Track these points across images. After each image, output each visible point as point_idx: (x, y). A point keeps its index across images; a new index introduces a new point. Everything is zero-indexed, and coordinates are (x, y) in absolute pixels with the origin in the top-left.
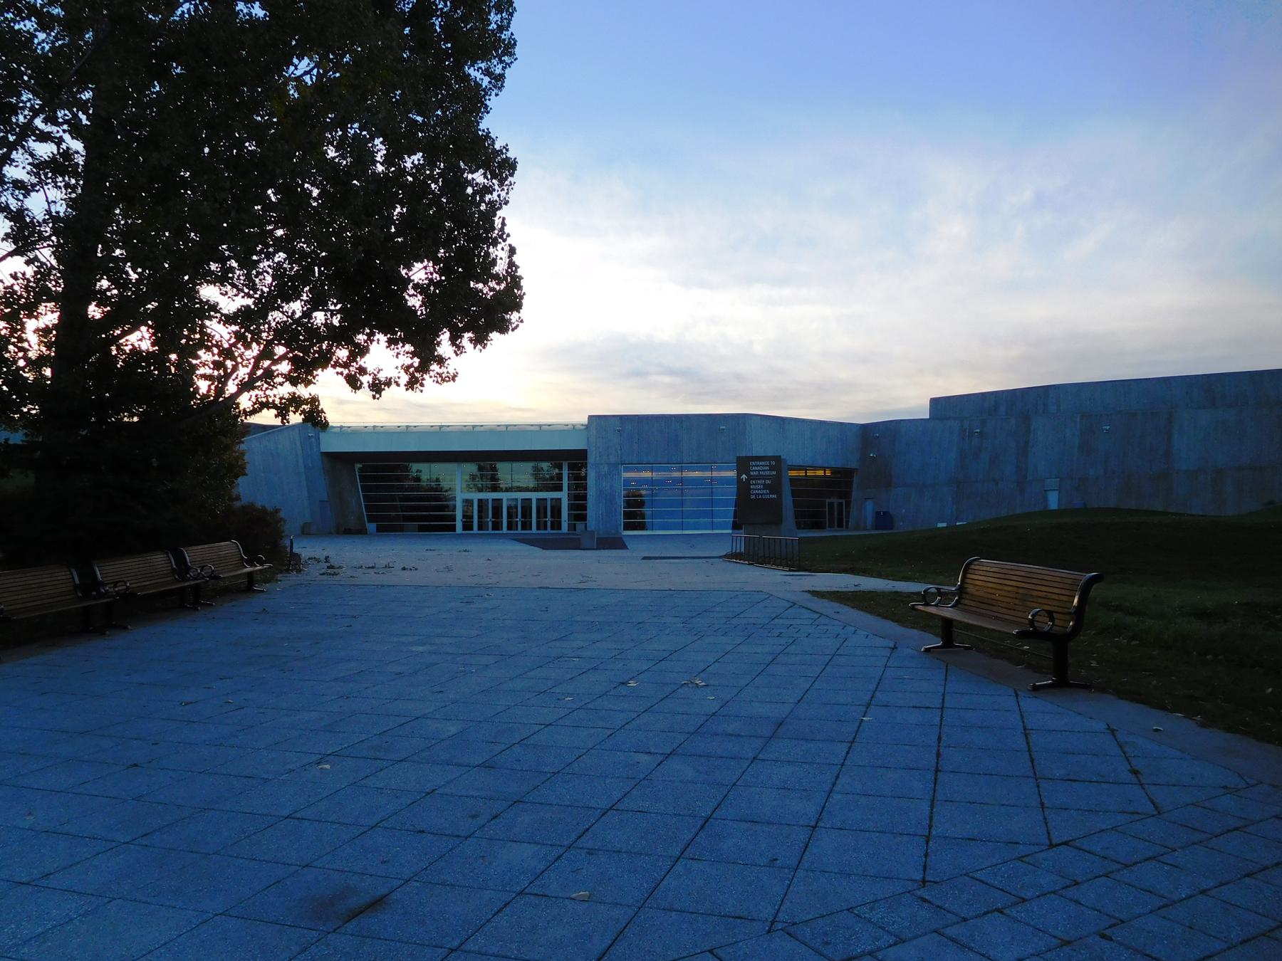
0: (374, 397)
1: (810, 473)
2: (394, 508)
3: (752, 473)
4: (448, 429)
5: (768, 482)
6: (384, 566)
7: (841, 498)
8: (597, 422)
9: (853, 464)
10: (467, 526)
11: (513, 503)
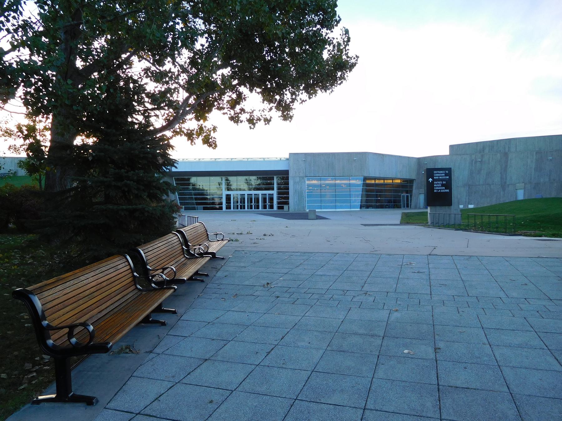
0: (251, 128)
1: (386, 181)
2: (192, 199)
3: (435, 178)
4: (219, 160)
5: (444, 182)
6: (246, 233)
7: (408, 193)
8: (294, 156)
9: (413, 177)
10: (228, 207)
11: (250, 196)
